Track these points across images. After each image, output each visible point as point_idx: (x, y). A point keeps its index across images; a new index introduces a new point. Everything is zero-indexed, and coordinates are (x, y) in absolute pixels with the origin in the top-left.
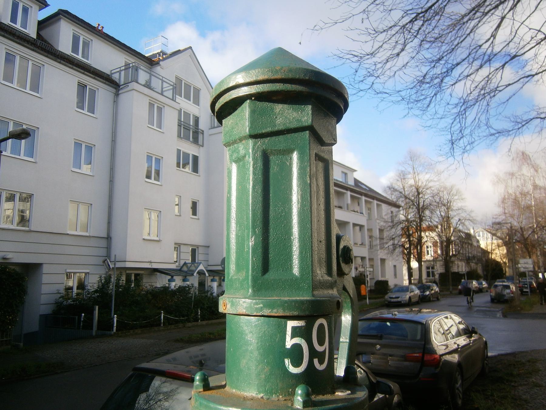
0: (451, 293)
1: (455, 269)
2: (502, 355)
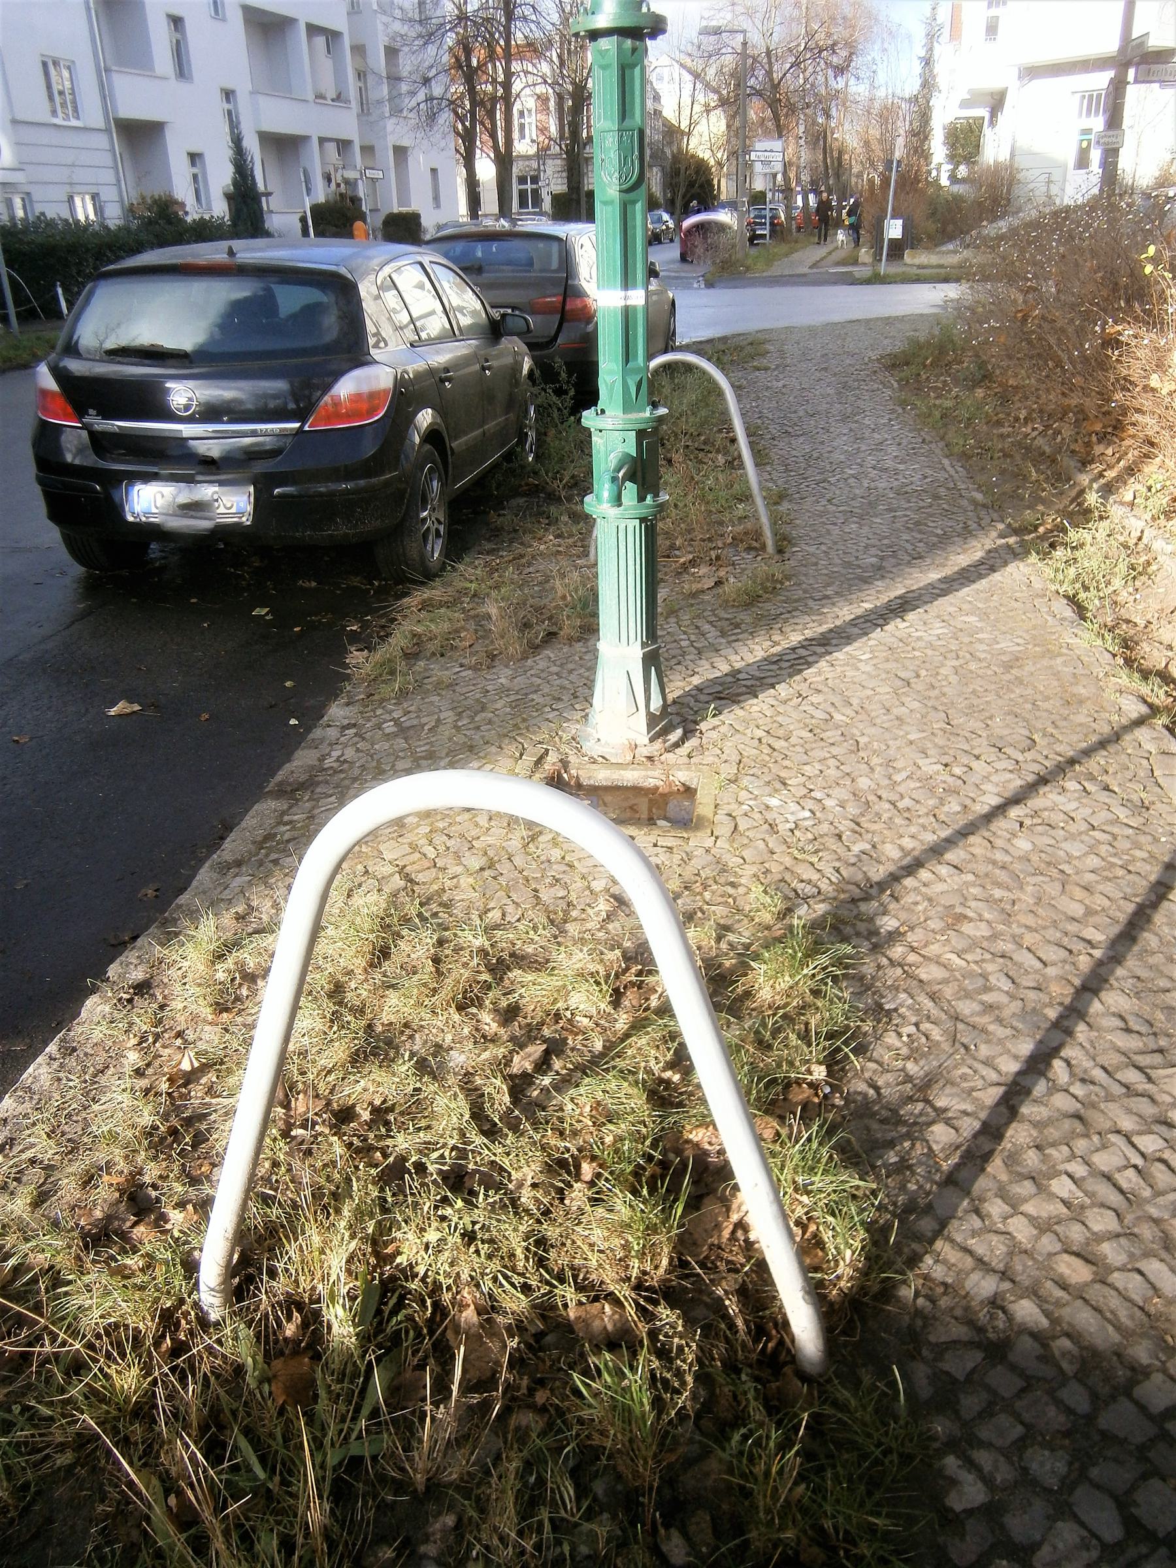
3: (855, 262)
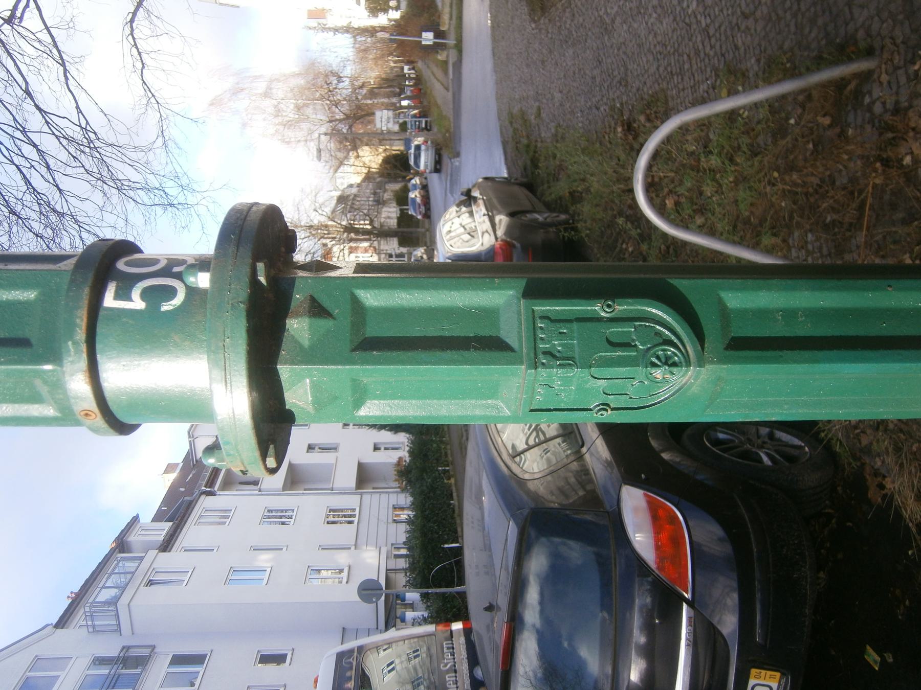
0: (428, 230)
1: (393, 223)
2: (506, 159)
3: (445, 63)
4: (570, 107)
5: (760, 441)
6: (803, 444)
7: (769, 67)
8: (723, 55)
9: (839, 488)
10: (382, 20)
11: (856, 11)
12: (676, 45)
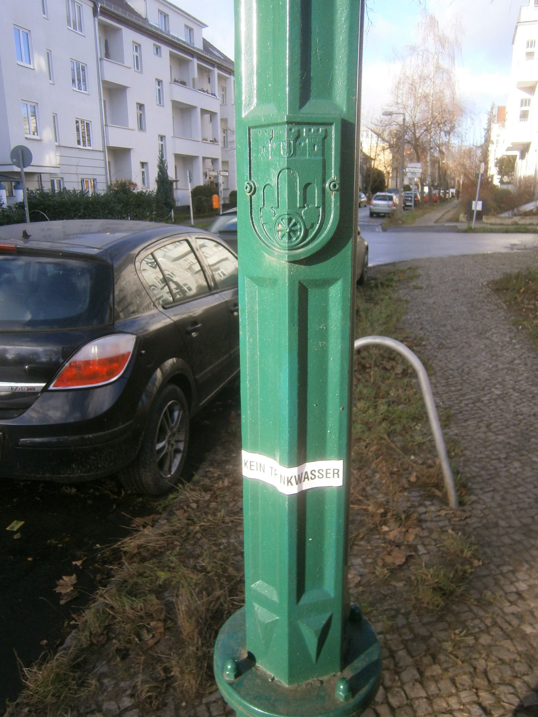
2: (381, 265)
3: (457, 220)
4: (422, 310)
5: (173, 442)
6: (172, 473)
7: (452, 441)
8: (461, 412)
9: (141, 499)
10: (493, 171)
11: (490, 495)
12: (468, 381)
